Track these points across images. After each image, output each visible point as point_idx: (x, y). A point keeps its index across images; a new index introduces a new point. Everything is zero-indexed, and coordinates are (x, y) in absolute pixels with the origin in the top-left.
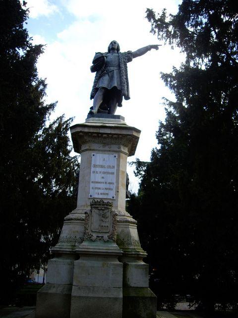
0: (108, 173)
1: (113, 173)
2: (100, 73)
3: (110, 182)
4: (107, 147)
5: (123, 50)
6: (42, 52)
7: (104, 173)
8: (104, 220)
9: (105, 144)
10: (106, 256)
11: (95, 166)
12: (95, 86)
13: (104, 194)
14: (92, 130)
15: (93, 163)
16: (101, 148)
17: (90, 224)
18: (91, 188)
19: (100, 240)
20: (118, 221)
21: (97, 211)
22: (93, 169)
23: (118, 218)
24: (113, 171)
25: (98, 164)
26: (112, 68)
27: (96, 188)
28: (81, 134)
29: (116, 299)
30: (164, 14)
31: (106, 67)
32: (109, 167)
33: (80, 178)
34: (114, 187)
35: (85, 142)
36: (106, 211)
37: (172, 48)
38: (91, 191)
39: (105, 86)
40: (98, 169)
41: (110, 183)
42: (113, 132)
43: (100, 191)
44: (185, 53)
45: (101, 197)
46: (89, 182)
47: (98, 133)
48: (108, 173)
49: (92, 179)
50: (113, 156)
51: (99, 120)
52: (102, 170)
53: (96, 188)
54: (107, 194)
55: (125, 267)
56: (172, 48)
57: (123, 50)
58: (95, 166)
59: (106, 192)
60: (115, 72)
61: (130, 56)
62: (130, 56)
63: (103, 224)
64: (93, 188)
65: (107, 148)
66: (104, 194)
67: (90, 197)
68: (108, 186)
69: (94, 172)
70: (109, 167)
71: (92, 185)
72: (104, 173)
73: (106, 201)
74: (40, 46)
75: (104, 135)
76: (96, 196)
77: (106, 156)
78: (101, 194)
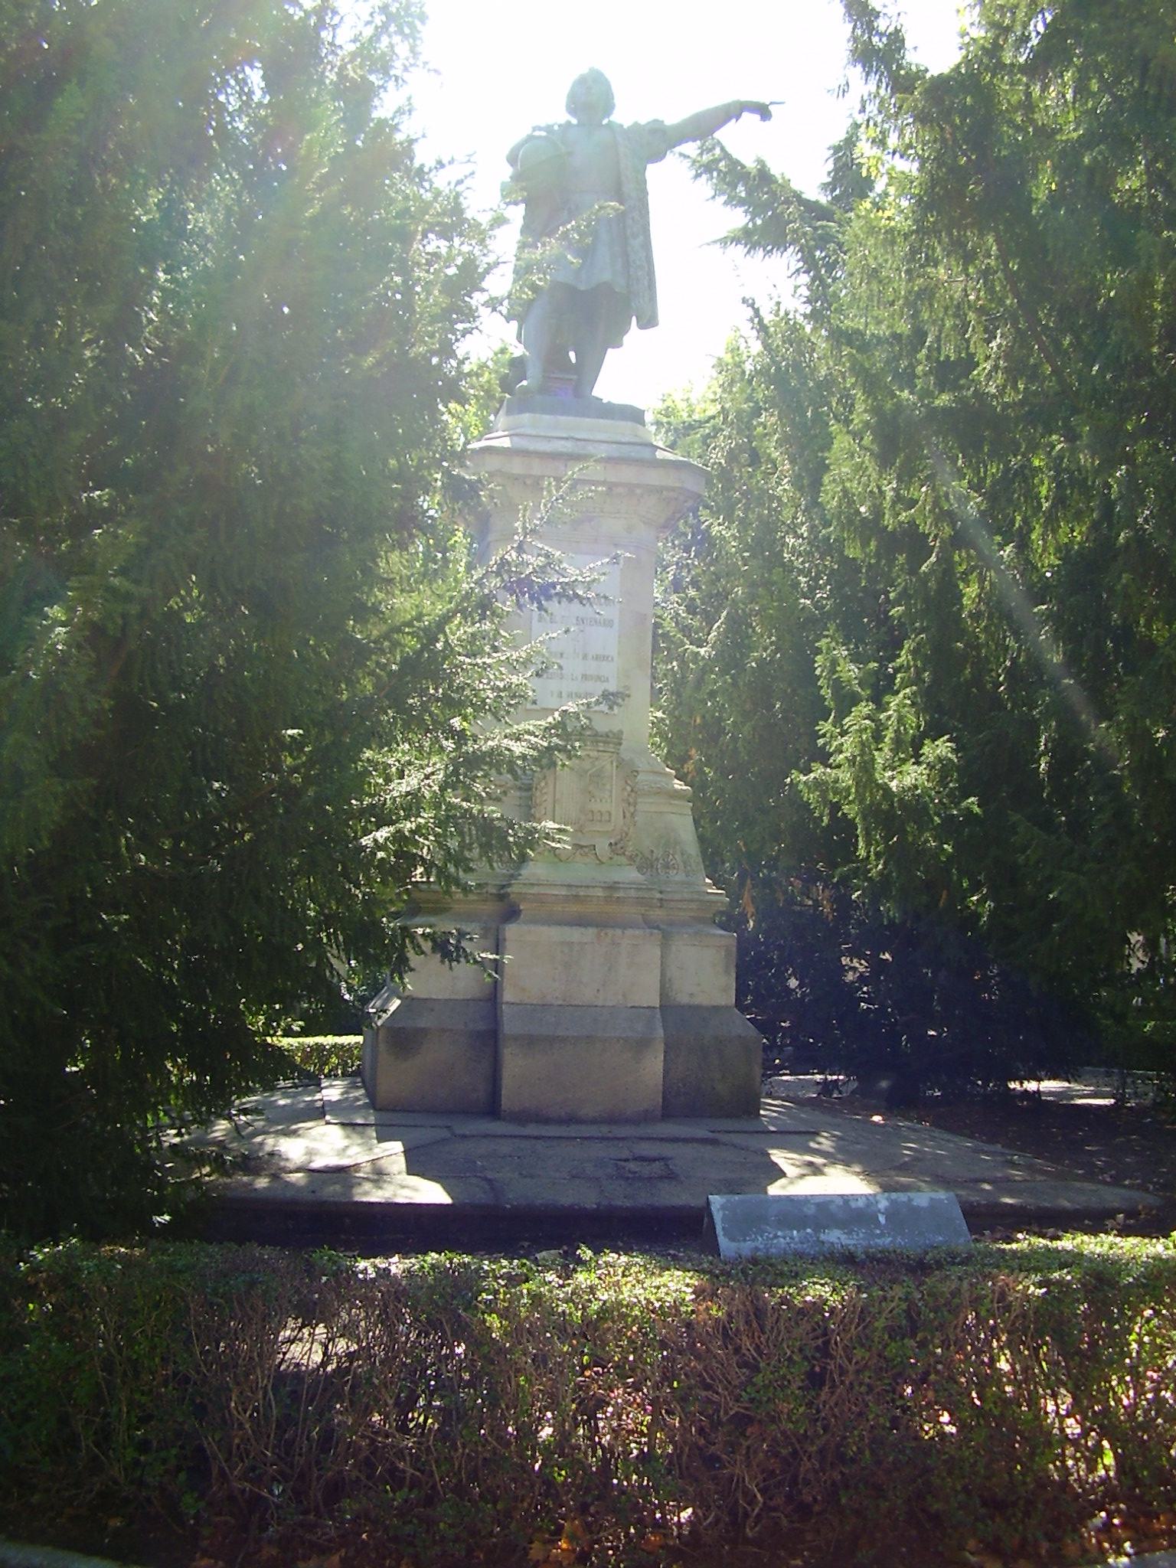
1: (608, 623)
5: (627, 113)
41: (597, 658)
57: (627, 113)
63: (596, 806)
69: (605, 658)
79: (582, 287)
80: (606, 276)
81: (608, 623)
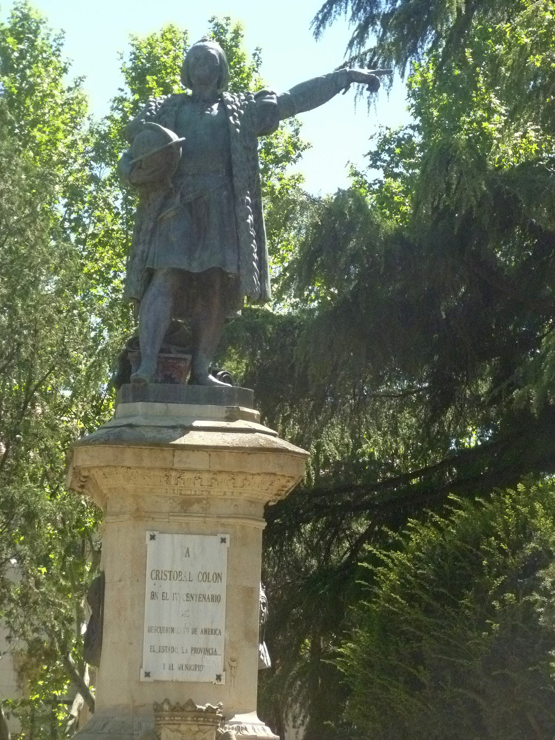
0: (203, 597)
1: (216, 599)
3: (208, 626)
7: (190, 597)
11: (158, 575)
13: (188, 668)
18: (146, 648)
22: (150, 585)
24: (216, 592)
25: (166, 566)
27: (162, 649)
30: (133, 45)
32: (206, 577)
33: (107, 580)
37: (8, 18)
38: (148, 656)
39: (184, 265)
40: (167, 586)
41: (206, 632)
43: (178, 659)
45: (180, 676)
46: (140, 628)
48: (203, 597)
49: (149, 621)
52: (185, 588)
53: (162, 649)
54: (198, 668)
56: (8, 18)
58: (158, 575)
59: (197, 659)
66: (188, 668)
67: (143, 678)
68: (201, 641)
70: (206, 577)
71: (150, 639)
72: (190, 597)
74: (217, 675)
76: (164, 675)
78: (181, 668)
81: (216, 599)
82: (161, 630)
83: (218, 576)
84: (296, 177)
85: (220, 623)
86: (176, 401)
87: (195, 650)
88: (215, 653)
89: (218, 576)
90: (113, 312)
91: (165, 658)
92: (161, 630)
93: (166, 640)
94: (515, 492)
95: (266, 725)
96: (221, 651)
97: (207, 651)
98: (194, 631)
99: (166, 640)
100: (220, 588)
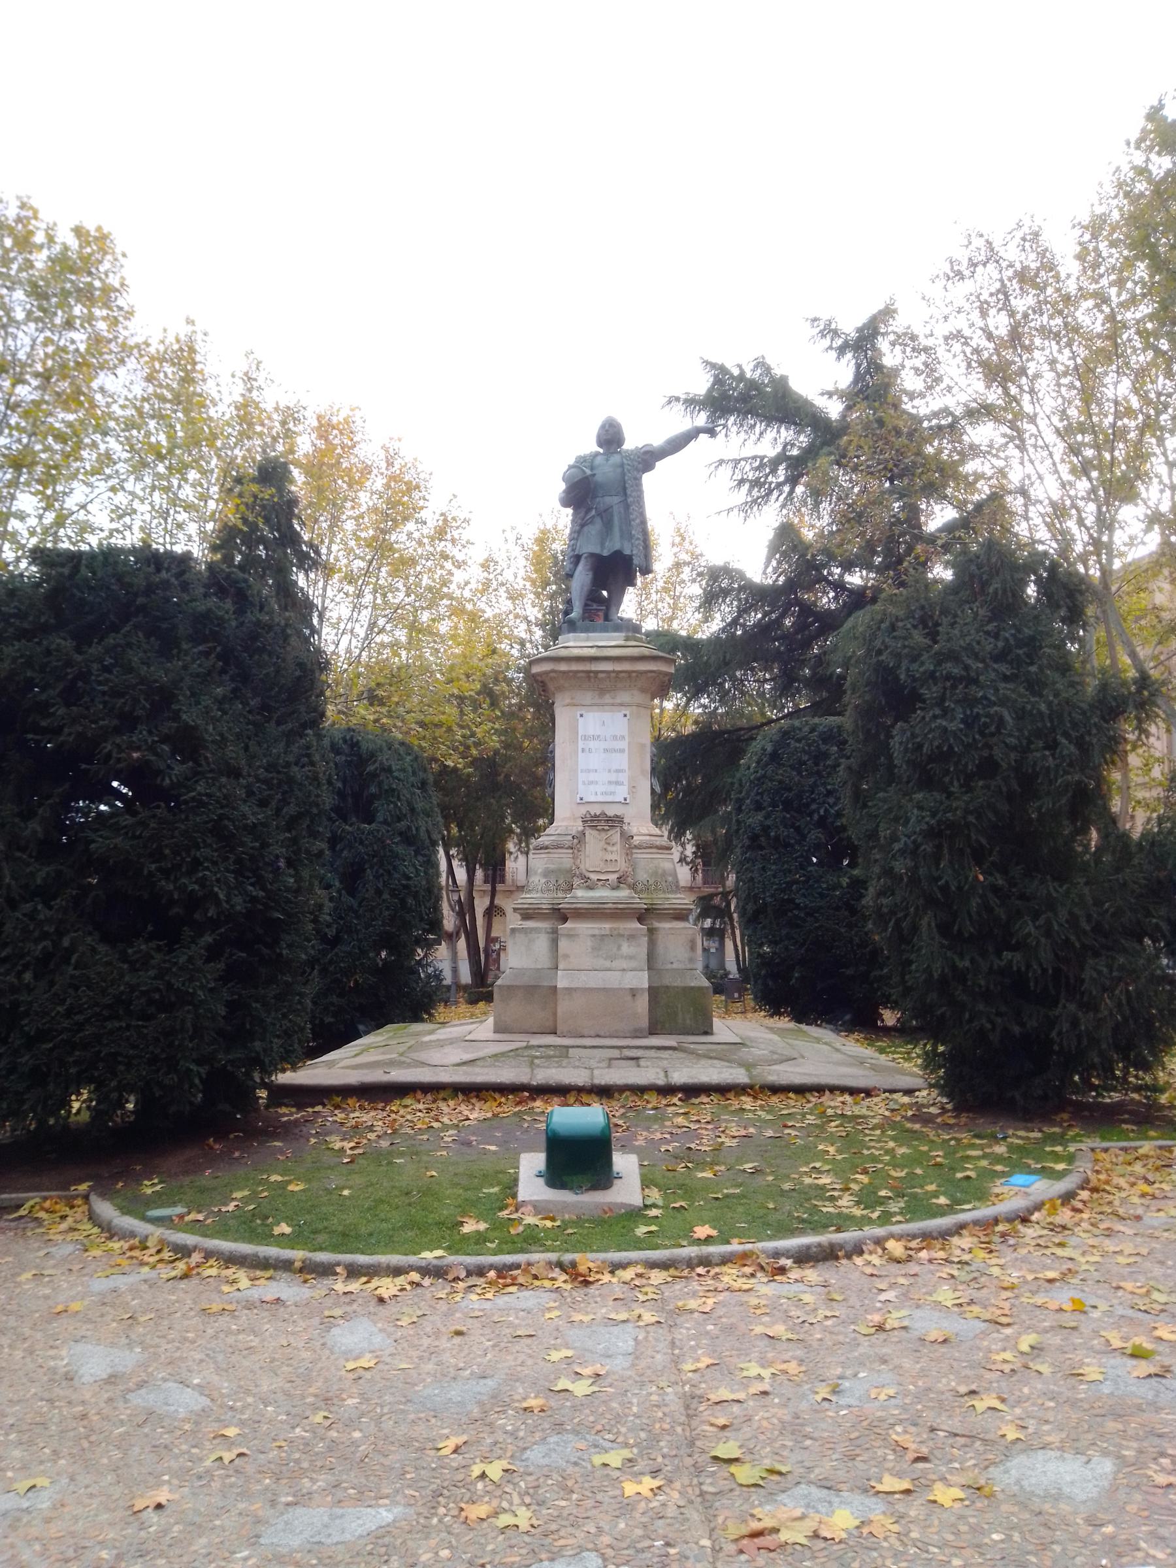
1: (622, 751)
2: (582, 515)
4: (607, 696)
5: (632, 442)
6: (720, 374)
7: (606, 750)
8: (609, 848)
9: (602, 692)
10: (617, 913)
11: (585, 738)
12: (573, 550)
13: (606, 793)
14: (575, 667)
15: (581, 733)
16: (597, 701)
17: (582, 857)
19: (603, 886)
20: (636, 847)
21: (595, 833)
22: (581, 744)
23: (637, 840)
25: (591, 732)
26: (608, 500)
27: (591, 783)
28: (552, 675)
29: (634, 993)
31: (594, 497)
32: (615, 738)
34: (624, 777)
35: (560, 689)
36: (610, 833)
38: (581, 787)
39: (597, 550)
40: (592, 744)
41: (617, 771)
42: (619, 667)
43: (600, 788)
44: (1119, 517)
47: (629, 672)
49: (582, 764)
50: (621, 715)
51: (588, 639)
52: (603, 745)
53: (591, 783)
55: (651, 931)
57: (632, 442)
58: (585, 738)
59: (612, 788)
60: (615, 508)
61: (648, 458)
62: (648, 458)
64: (584, 783)
65: (607, 699)
66: (606, 793)
68: (613, 777)
70: (615, 738)
71: (582, 777)
72: (606, 750)
73: (611, 811)
75: (600, 675)
77: (606, 716)
79: (605, 553)
80: (617, 547)
81: (622, 751)
82: (589, 771)
83: (623, 737)
84: (678, 540)
85: (625, 766)
86: (594, 631)
87: (610, 783)
88: (622, 784)
89: (623, 737)
90: (90, 311)
91: (592, 788)
92: (589, 771)
93: (592, 777)
94: (143, 673)
95: (402, 1098)
96: (626, 783)
97: (617, 783)
98: (610, 771)
99: (592, 777)
100: (623, 745)
